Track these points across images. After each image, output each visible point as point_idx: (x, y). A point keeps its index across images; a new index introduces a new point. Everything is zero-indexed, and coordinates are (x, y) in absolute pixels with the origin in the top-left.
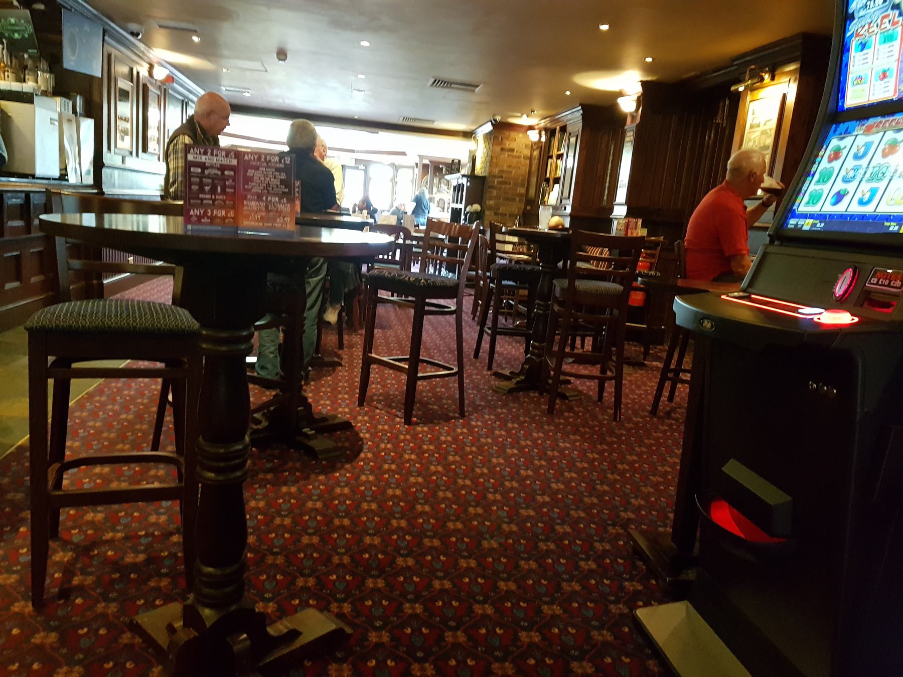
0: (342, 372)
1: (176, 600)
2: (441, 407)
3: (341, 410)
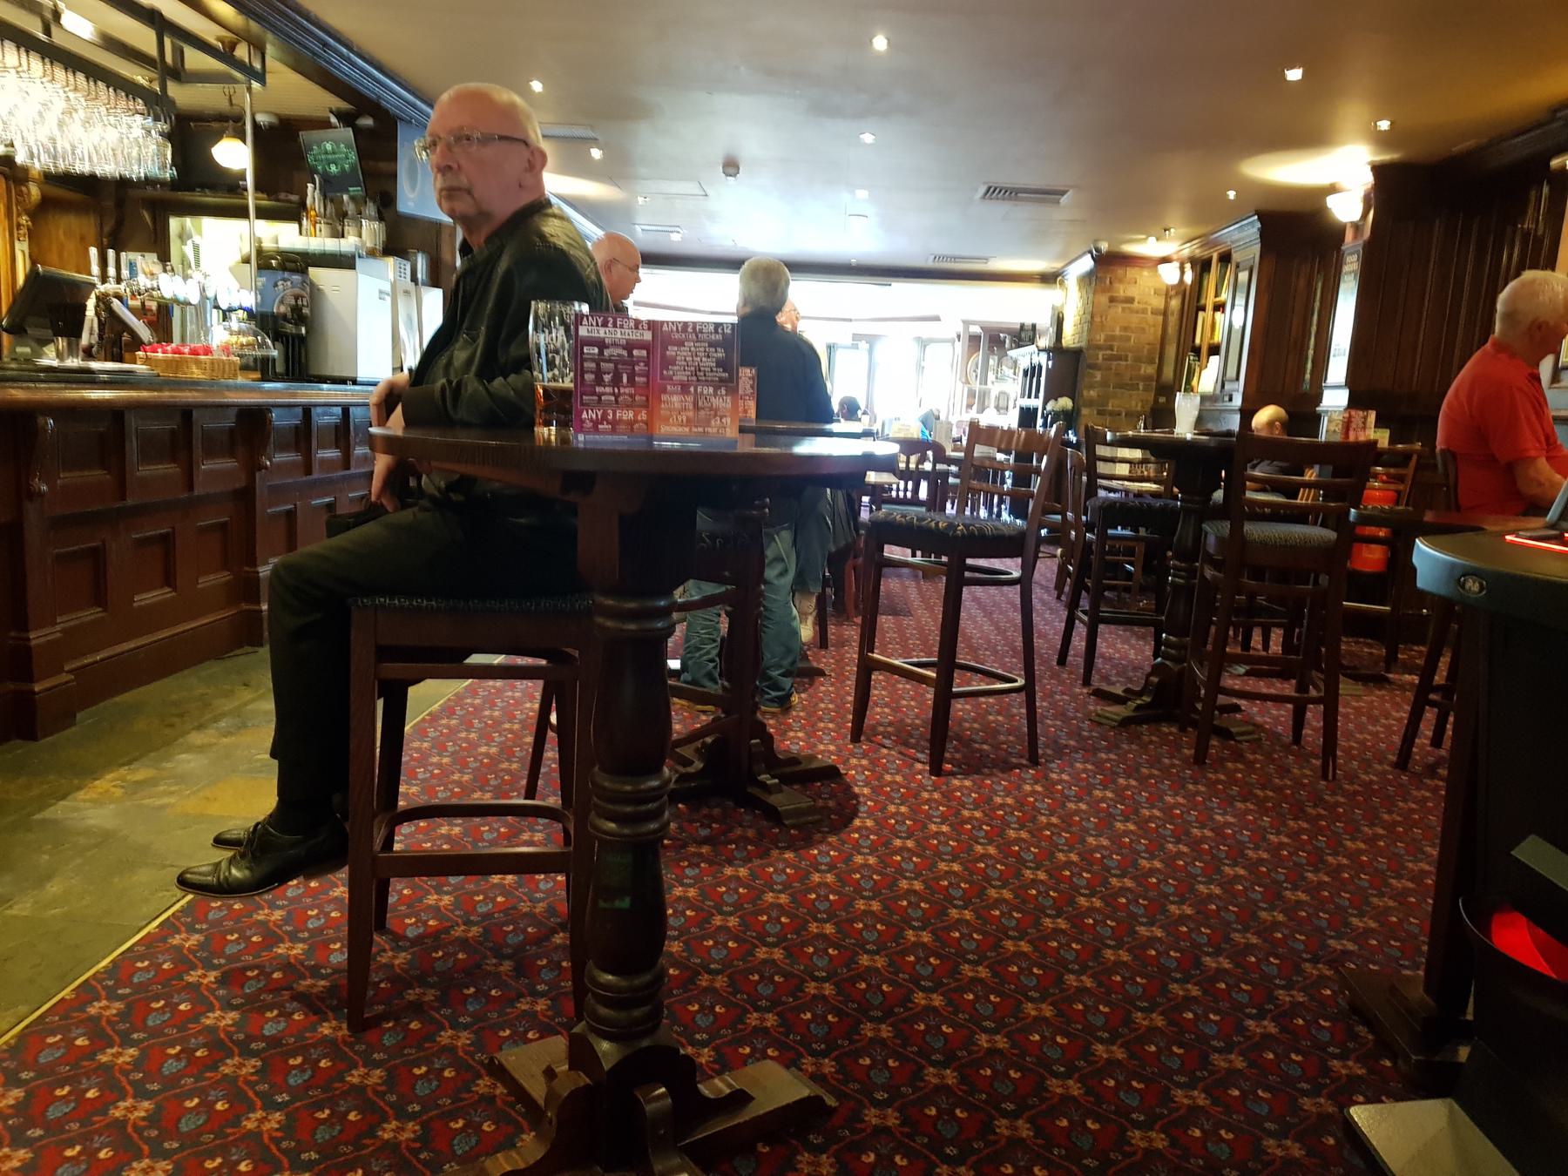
0: (824, 687)
1: (558, 1033)
2: (997, 747)
3: (822, 747)
